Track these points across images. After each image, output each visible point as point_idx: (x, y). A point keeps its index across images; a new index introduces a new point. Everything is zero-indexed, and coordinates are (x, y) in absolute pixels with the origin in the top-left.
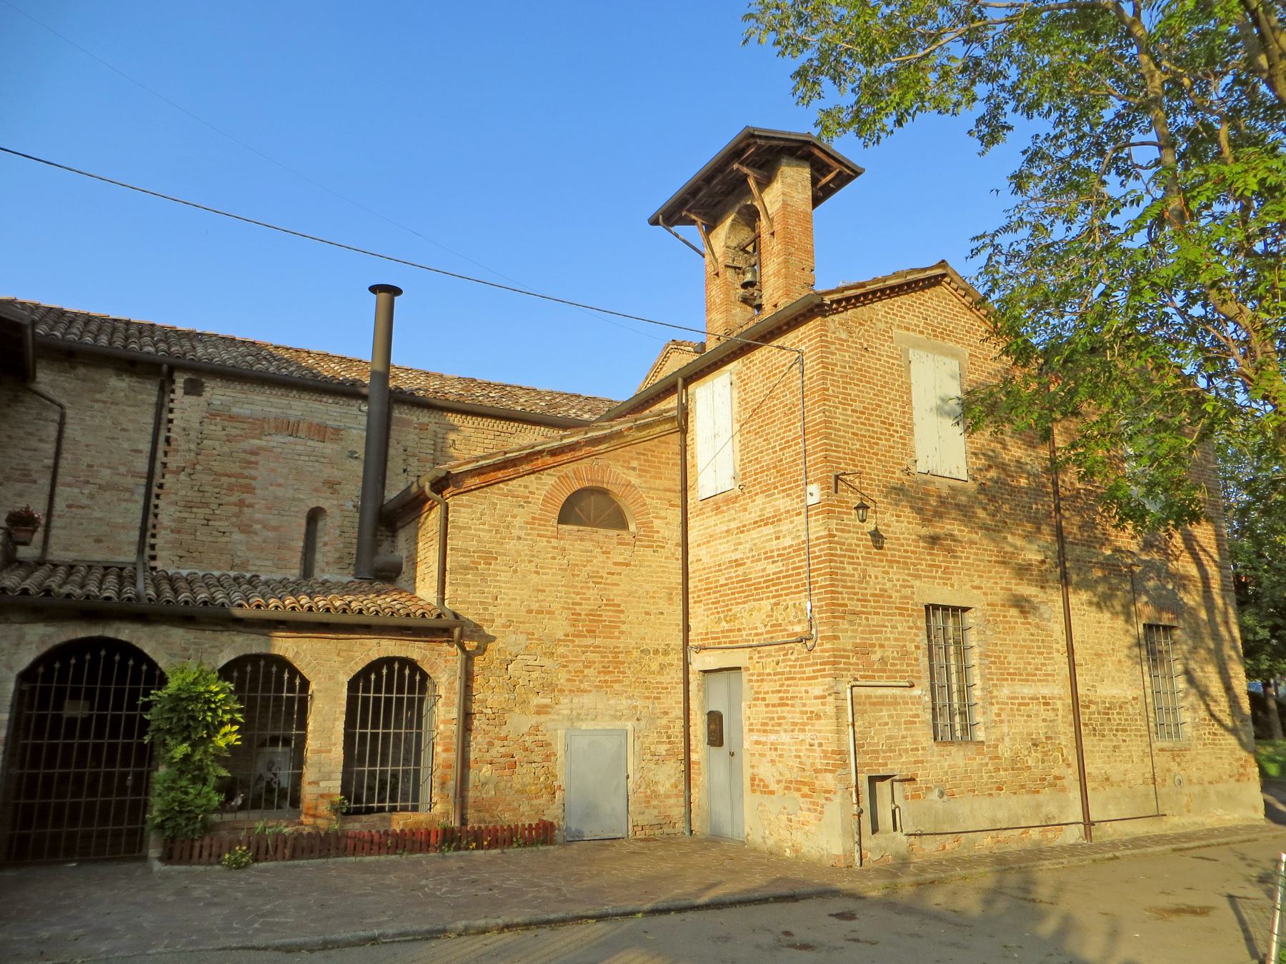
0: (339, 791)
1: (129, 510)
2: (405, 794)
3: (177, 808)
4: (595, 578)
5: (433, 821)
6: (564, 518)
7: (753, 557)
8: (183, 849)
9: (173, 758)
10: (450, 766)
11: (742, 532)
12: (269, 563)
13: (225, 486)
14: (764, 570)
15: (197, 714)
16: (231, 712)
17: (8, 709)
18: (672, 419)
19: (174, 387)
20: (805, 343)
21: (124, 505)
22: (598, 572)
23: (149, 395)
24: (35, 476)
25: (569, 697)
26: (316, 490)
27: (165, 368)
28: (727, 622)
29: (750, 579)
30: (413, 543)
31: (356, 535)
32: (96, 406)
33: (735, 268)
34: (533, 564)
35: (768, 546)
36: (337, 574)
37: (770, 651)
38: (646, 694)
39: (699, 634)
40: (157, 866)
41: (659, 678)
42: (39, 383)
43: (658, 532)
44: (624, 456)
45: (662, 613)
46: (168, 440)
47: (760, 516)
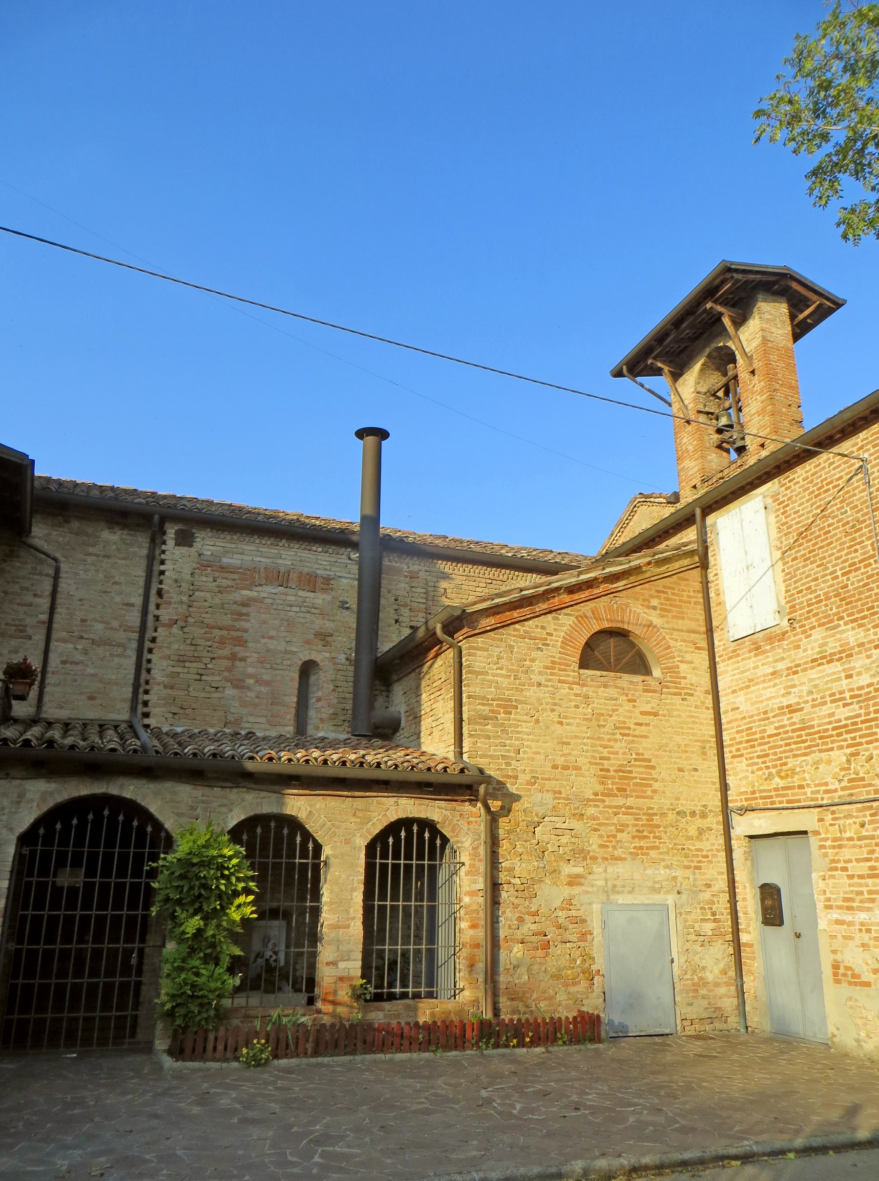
0: (359, 973)
1: (121, 666)
2: (417, 976)
3: (189, 993)
4: (622, 729)
5: (460, 1012)
6: (584, 664)
7: (813, 700)
8: (195, 1040)
9: (184, 933)
10: (478, 946)
11: (796, 673)
12: (263, 720)
13: (217, 639)
14: (832, 714)
15: (209, 882)
16: (247, 879)
17: (8, 875)
18: (692, 553)
19: (165, 538)
20: (868, 450)
21: (117, 660)
22: (625, 723)
23: (141, 547)
24: (30, 631)
25: (603, 866)
26: (308, 642)
27: (156, 518)
28: (781, 778)
29: (813, 727)
30: (413, 696)
31: (351, 690)
32: (90, 559)
33: (708, 413)
34: (556, 713)
35: (835, 687)
36: (332, 731)
37: (851, 810)
38: (686, 863)
39: (741, 793)
40: (168, 1062)
41: (699, 845)
42: (35, 537)
43: (685, 678)
44: (643, 594)
45: (696, 770)
46: (160, 593)
47: (820, 652)
